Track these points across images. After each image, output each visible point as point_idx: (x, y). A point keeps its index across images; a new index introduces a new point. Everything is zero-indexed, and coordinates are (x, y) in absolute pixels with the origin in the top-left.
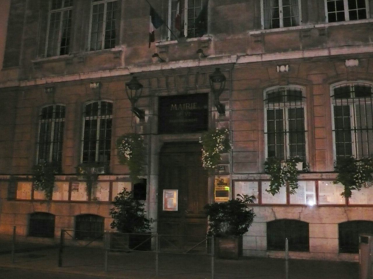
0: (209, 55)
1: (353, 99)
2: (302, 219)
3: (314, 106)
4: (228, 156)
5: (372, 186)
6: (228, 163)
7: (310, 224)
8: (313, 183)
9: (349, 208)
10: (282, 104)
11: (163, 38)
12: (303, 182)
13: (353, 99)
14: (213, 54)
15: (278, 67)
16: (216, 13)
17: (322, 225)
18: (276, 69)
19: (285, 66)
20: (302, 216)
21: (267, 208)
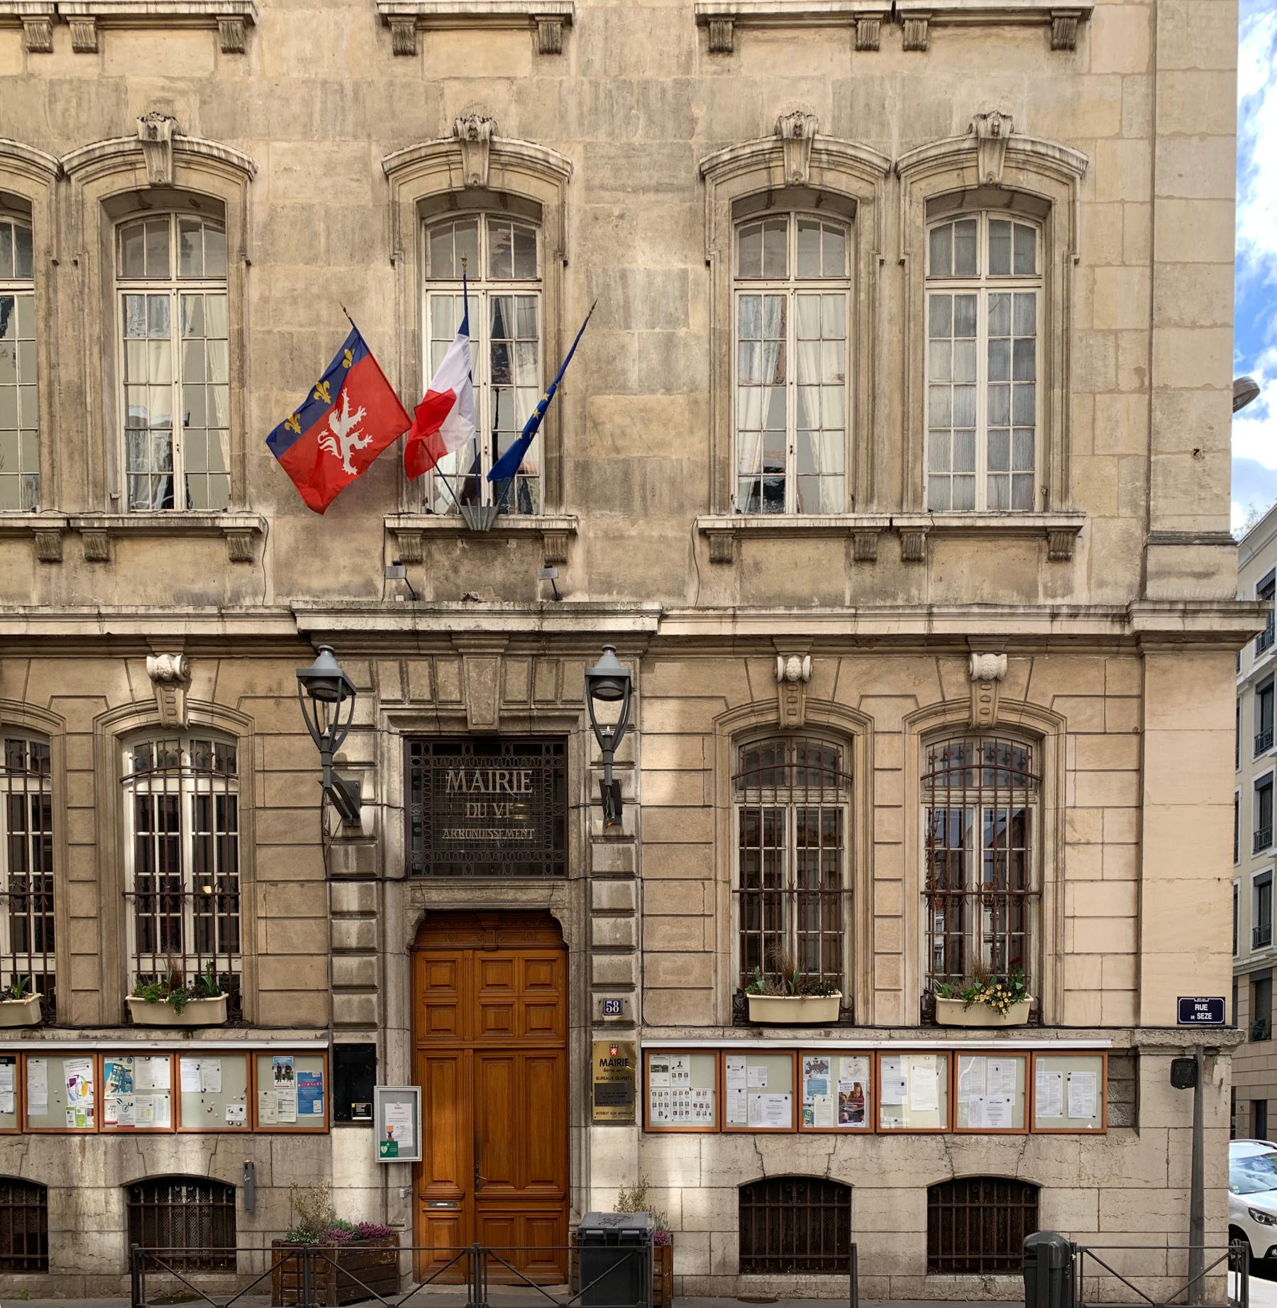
0: (568, 594)
1: (980, 790)
2: (835, 1175)
3: (874, 916)
4: (629, 965)
5: (4, 990)
6: (629, 987)
7: (855, 1194)
8: (1015, 1066)
9: (957, 1139)
10: (783, 795)
11: (412, 500)
12: (343, 983)
13: (980, 790)
14: (582, 590)
15: (780, 659)
16: (589, 420)
17: (885, 1192)
18: (776, 665)
19: (802, 658)
20: (834, 1166)
21: (741, 1140)
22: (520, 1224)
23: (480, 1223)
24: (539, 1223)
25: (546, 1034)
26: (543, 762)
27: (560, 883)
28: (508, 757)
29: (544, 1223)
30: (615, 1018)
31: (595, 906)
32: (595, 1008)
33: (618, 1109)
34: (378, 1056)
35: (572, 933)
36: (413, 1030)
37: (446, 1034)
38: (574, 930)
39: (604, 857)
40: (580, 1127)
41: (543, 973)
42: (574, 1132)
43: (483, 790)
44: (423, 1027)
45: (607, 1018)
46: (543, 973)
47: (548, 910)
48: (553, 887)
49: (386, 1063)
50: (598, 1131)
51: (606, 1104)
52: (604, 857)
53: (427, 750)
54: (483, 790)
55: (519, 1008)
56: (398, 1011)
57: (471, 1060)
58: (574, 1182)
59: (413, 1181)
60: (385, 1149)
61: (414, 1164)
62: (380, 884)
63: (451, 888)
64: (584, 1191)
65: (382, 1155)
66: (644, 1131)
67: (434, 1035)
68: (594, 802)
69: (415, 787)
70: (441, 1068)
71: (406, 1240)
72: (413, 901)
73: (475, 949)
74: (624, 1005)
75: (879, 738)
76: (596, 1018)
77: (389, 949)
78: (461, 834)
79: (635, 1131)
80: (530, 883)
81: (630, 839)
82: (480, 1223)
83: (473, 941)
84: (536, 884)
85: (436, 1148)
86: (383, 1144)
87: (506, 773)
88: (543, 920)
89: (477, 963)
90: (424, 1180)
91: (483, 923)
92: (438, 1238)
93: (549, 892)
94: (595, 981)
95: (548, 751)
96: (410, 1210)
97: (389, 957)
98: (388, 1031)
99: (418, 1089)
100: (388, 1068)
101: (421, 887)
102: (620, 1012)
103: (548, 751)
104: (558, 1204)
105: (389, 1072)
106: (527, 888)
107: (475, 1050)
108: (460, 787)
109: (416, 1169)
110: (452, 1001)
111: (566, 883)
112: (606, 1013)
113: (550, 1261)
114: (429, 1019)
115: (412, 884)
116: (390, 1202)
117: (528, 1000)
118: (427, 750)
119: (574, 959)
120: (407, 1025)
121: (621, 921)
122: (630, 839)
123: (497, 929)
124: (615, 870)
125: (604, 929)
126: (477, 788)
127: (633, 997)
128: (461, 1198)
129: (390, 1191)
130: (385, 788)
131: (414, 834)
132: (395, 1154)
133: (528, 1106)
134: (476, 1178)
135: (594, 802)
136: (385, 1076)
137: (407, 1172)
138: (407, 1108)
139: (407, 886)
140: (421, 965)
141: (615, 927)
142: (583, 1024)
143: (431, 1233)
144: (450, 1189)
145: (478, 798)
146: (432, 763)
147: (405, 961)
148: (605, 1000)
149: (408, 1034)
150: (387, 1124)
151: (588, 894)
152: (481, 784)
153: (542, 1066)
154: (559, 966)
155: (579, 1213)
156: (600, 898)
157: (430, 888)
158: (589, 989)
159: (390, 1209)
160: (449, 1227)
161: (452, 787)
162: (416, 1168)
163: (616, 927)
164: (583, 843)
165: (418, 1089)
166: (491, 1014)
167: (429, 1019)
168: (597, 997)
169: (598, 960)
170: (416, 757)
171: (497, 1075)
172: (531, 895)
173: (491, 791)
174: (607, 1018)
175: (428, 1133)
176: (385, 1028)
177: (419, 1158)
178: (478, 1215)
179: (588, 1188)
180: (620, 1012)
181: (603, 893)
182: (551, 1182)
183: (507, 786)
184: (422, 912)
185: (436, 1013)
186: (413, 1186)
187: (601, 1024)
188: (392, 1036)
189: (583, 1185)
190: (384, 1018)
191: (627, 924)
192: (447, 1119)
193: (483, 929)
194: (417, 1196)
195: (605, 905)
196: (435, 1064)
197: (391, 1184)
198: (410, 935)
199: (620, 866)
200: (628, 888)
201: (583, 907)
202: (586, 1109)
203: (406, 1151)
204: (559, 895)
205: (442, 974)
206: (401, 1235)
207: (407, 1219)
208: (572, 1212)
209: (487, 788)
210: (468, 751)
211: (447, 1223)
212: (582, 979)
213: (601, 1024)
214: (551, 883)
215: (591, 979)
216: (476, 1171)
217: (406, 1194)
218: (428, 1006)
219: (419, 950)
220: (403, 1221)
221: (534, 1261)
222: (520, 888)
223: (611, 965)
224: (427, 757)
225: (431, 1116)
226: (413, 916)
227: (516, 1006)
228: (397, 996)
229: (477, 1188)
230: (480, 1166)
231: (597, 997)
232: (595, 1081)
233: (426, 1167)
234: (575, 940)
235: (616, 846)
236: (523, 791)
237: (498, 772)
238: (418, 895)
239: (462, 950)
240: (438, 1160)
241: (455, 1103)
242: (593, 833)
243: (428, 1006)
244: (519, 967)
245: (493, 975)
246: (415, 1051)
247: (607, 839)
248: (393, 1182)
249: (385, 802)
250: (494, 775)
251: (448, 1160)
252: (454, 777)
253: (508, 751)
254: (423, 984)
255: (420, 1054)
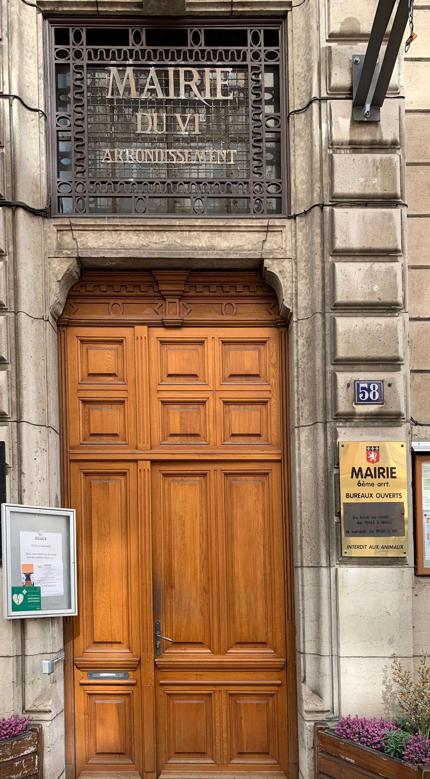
6: (393, 363)
22: (221, 702)
23: (163, 700)
24: (248, 701)
25: (254, 440)
26: (249, 56)
27: (277, 222)
28: (196, 48)
29: (254, 701)
30: (372, 408)
31: (339, 244)
32: (342, 393)
33: (381, 541)
34: (8, 461)
35: (296, 290)
36: (63, 432)
37: (111, 440)
38: (302, 287)
39: (353, 174)
40: (318, 567)
41: (248, 360)
42: (305, 577)
43: (161, 96)
44: (77, 431)
45: (360, 409)
46: (248, 360)
47: (261, 261)
48: (267, 230)
49: (21, 473)
50: (350, 574)
51: (363, 533)
52: (353, 174)
53: (78, 38)
54: (161, 96)
55: (214, 405)
56: (40, 400)
57: (148, 476)
58: (307, 644)
59: (65, 643)
60: (19, 599)
61: (66, 620)
62: (9, 213)
63: (116, 229)
64: (326, 662)
65: (15, 608)
66: (416, 574)
67: (96, 440)
68: (336, 93)
69: (61, 104)
70: (105, 487)
71: (53, 732)
72: (60, 247)
73: (151, 325)
74: (387, 390)
75: (21, 654)
76: (343, 407)
77: (24, 307)
78: (130, 154)
79: (409, 572)
80: (234, 223)
81: (393, 146)
82: (163, 700)
83: (148, 314)
84: (243, 223)
85: (97, 596)
86: (16, 590)
87: (194, 71)
88: (254, 280)
89: (155, 345)
90: (81, 642)
91: (163, 287)
92: (102, 721)
93: (262, 236)
94: (341, 353)
95: (256, 40)
96: (60, 685)
97: (24, 319)
98: (24, 426)
99: (72, 514)
100: (25, 479)
101: (71, 228)
102: (381, 401)
103: (256, 40)
104: (276, 674)
105: (25, 485)
106: (229, 229)
107: (153, 462)
108: (127, 89)
109: (70, 627)
110: (122, 395)
111: (288, 223)
112: (359, 402)
113: (265, 753)
114: (87, 420)
115: (58, 222)
116: (29, 678)
117: (228, 396)
118: (78, 38)
119: (300, 332)
120: (54, 421)
121: (380, 267)
122: (393, 146)
123: (181, 297)
124: (370, 191)
125: (354, 280)
126: (153, 91)
127: (400, 378)
128: (136, 666)
129: (29, 661)
130: (15, 73)
131: (61, 167)
132: (37, 606)
133: (230, 539)
134: (156, 638)
135: (336, 93)
136: (20, 491)
137: (56, 634)
138: (56, 540)
139: (51, 225)
140: (74, 347)
141: (371, 274)
142: (320, 418)
143: (92, 715)
144: (118, 654)
145: (157, 105)
146: (85, 55)
147: (49, 333)
148: (357, 383)
149: (54, 438)
150: (24, 561)
151: (328, 232)
152: (157, 86)
153: (249, 488)
154: (272, 351)
155: (317, 692)
156: (346, 234)
157: (85, 228)
158: (330, 368)
159: (29, 688)
160: (118, 706)
161: (115, 90)
162: (70, 626)
163: (372, 276)
164: (317, 157)
165: (72, 514)
166: (175, 412)
167: (87, 420)
168: (343, 378)
169: (344, 324)
170: (61, 47)
171: (185, 498)
172: (235, 241)
173: (172, 96)
174: (360, 409)
175: (86, 577)
176: (19, 421)
177: (73, 612)
178: (160, 690)
179: (336, 657)
180: (381, 401)
181: (352, 226)
182: (264, 644)
183: (195, 89)
184: (74, 262)
185: (97, 413)
186: (65, 649)
187: (348, 418)
188: (31, 435)
189: (326, 650)
190: (18, 408)
191: (390, 271)
192: (113, 554)
193: (163, 298)
194: (71, 664)
195: (355, 243)
196: (96, 481)
197: (29, 651)
198: (56, 295)
199: (377, 186)
200: (391, 217)
201: (318, 249)
202: (328, 542)
203: (54, 602)
204: (274, 241)
205: (103, 359)
206: (45, 726)
207: (55, 702)
208: (305, 690)
209: (167, 92)
210: (137, 39)
211: (114, 701)
212: (319, 355)
213: (348, 418)
214: (265, 222)
215: (334, 351)
216: (157, 627)
217: (53, 666)
218: (85, 402)
219: (68, 325)
220: (49, 705)
221: (241, 754)
222: (218, 230)
223: (366, 331)
224: (78, 47)
225: (91, 553)
226: (61, 267)
227: (210, 404)
228: (37, 378)
229: (158, 651)
230: (162, 622)
231: (343, 378)
232: (344, 500)
233: (83, 624)
234: (303, 301)
235: (370, 157)
236: (219, 96)
237: (182, 70)
238: (67, 238)
239: (131, 325)
240: (101, 612)
241: (126, 533)
242: (335, 138)
243: (85, 402)
244: (213, 349)
245: (176, 360)
246: (67, 461)
247: (355, 146)
248: (32, 648)
249: (15, 92)
250: (177, 74)
251: (115, 613)
252: (118, 79)
253: (196, 40)
254: (76, 371)
255: (75, 467)
